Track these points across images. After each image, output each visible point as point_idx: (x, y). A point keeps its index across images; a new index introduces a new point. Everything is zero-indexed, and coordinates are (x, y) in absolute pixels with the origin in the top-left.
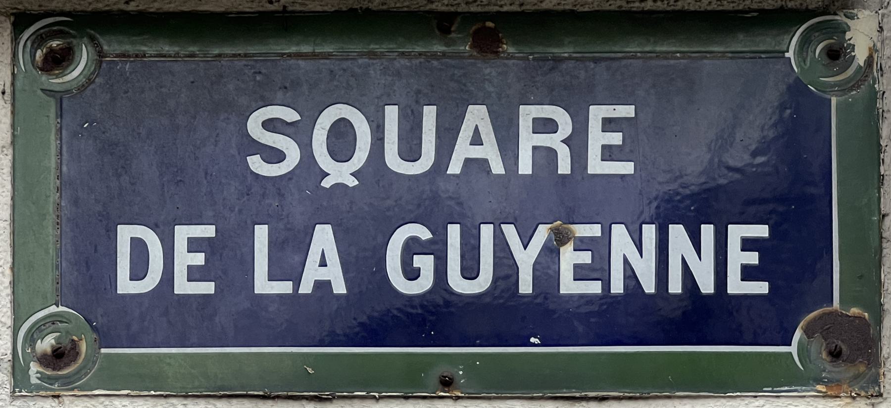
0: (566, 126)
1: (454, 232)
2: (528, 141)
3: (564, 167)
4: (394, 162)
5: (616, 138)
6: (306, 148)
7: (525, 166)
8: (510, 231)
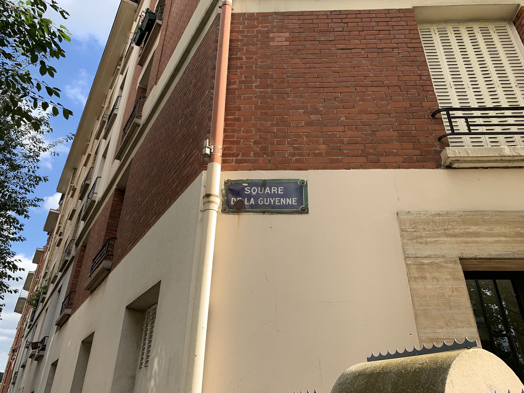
0: (276, 189)
1: (265, 199)
2: (273, 190)
3: (276, 193)
4: (259, 192)
5: (295, 201)
6: (251, 191)
7: (272, 193)
8: (271, 199)
